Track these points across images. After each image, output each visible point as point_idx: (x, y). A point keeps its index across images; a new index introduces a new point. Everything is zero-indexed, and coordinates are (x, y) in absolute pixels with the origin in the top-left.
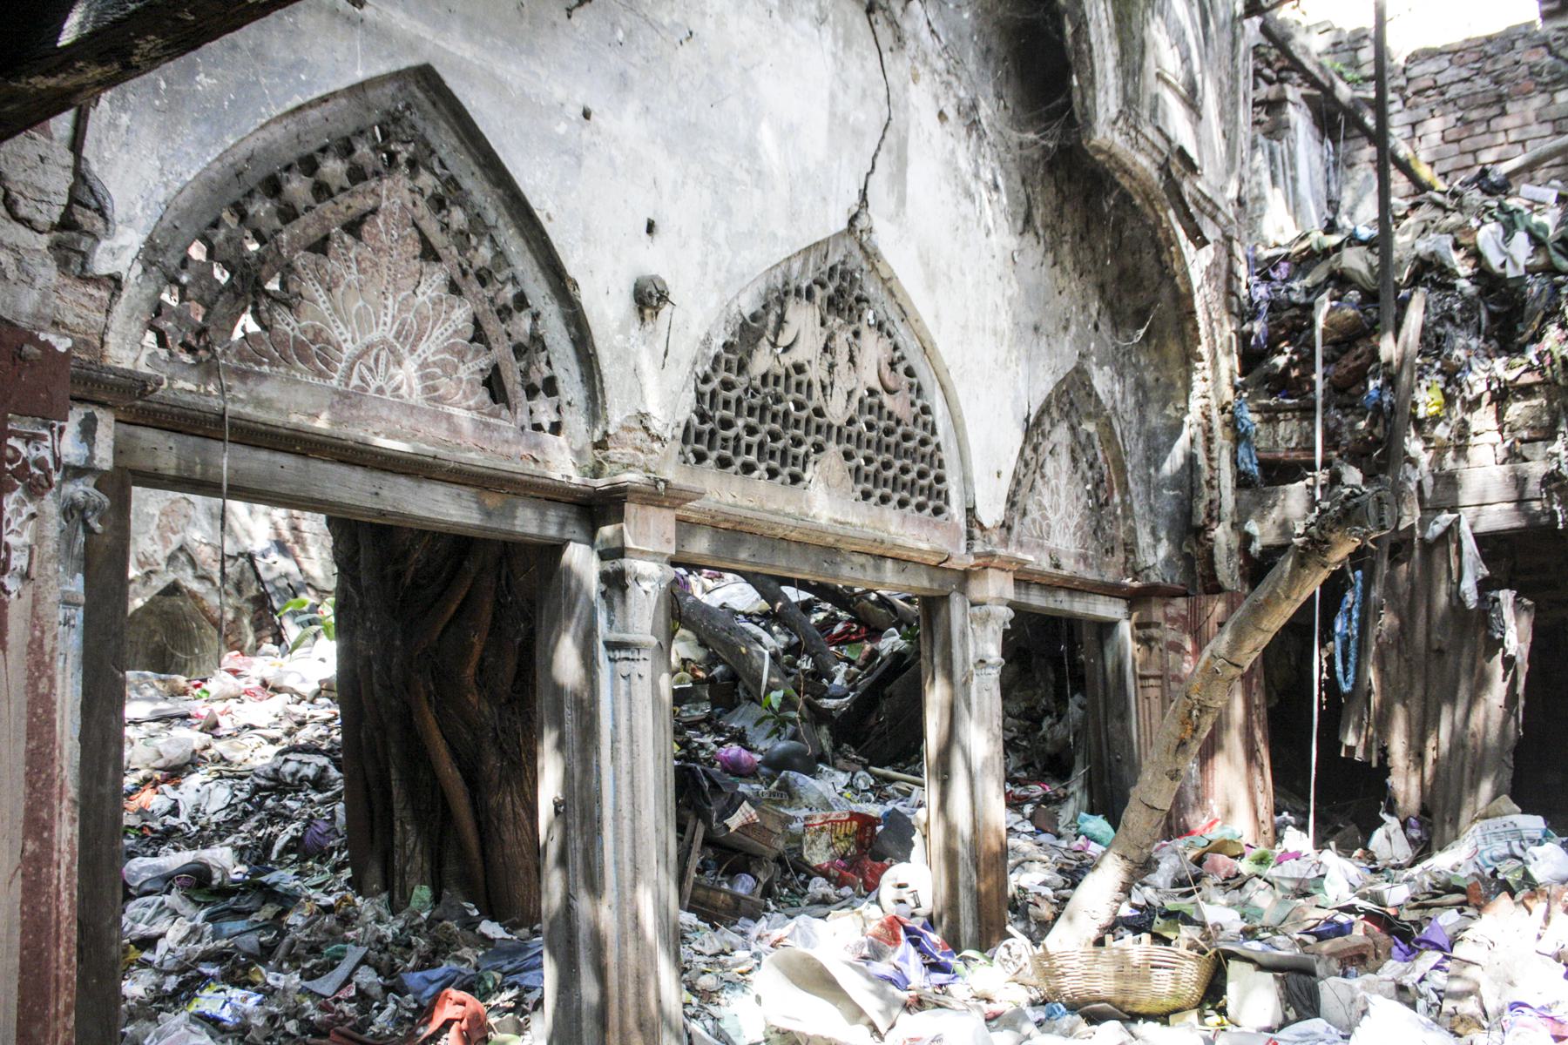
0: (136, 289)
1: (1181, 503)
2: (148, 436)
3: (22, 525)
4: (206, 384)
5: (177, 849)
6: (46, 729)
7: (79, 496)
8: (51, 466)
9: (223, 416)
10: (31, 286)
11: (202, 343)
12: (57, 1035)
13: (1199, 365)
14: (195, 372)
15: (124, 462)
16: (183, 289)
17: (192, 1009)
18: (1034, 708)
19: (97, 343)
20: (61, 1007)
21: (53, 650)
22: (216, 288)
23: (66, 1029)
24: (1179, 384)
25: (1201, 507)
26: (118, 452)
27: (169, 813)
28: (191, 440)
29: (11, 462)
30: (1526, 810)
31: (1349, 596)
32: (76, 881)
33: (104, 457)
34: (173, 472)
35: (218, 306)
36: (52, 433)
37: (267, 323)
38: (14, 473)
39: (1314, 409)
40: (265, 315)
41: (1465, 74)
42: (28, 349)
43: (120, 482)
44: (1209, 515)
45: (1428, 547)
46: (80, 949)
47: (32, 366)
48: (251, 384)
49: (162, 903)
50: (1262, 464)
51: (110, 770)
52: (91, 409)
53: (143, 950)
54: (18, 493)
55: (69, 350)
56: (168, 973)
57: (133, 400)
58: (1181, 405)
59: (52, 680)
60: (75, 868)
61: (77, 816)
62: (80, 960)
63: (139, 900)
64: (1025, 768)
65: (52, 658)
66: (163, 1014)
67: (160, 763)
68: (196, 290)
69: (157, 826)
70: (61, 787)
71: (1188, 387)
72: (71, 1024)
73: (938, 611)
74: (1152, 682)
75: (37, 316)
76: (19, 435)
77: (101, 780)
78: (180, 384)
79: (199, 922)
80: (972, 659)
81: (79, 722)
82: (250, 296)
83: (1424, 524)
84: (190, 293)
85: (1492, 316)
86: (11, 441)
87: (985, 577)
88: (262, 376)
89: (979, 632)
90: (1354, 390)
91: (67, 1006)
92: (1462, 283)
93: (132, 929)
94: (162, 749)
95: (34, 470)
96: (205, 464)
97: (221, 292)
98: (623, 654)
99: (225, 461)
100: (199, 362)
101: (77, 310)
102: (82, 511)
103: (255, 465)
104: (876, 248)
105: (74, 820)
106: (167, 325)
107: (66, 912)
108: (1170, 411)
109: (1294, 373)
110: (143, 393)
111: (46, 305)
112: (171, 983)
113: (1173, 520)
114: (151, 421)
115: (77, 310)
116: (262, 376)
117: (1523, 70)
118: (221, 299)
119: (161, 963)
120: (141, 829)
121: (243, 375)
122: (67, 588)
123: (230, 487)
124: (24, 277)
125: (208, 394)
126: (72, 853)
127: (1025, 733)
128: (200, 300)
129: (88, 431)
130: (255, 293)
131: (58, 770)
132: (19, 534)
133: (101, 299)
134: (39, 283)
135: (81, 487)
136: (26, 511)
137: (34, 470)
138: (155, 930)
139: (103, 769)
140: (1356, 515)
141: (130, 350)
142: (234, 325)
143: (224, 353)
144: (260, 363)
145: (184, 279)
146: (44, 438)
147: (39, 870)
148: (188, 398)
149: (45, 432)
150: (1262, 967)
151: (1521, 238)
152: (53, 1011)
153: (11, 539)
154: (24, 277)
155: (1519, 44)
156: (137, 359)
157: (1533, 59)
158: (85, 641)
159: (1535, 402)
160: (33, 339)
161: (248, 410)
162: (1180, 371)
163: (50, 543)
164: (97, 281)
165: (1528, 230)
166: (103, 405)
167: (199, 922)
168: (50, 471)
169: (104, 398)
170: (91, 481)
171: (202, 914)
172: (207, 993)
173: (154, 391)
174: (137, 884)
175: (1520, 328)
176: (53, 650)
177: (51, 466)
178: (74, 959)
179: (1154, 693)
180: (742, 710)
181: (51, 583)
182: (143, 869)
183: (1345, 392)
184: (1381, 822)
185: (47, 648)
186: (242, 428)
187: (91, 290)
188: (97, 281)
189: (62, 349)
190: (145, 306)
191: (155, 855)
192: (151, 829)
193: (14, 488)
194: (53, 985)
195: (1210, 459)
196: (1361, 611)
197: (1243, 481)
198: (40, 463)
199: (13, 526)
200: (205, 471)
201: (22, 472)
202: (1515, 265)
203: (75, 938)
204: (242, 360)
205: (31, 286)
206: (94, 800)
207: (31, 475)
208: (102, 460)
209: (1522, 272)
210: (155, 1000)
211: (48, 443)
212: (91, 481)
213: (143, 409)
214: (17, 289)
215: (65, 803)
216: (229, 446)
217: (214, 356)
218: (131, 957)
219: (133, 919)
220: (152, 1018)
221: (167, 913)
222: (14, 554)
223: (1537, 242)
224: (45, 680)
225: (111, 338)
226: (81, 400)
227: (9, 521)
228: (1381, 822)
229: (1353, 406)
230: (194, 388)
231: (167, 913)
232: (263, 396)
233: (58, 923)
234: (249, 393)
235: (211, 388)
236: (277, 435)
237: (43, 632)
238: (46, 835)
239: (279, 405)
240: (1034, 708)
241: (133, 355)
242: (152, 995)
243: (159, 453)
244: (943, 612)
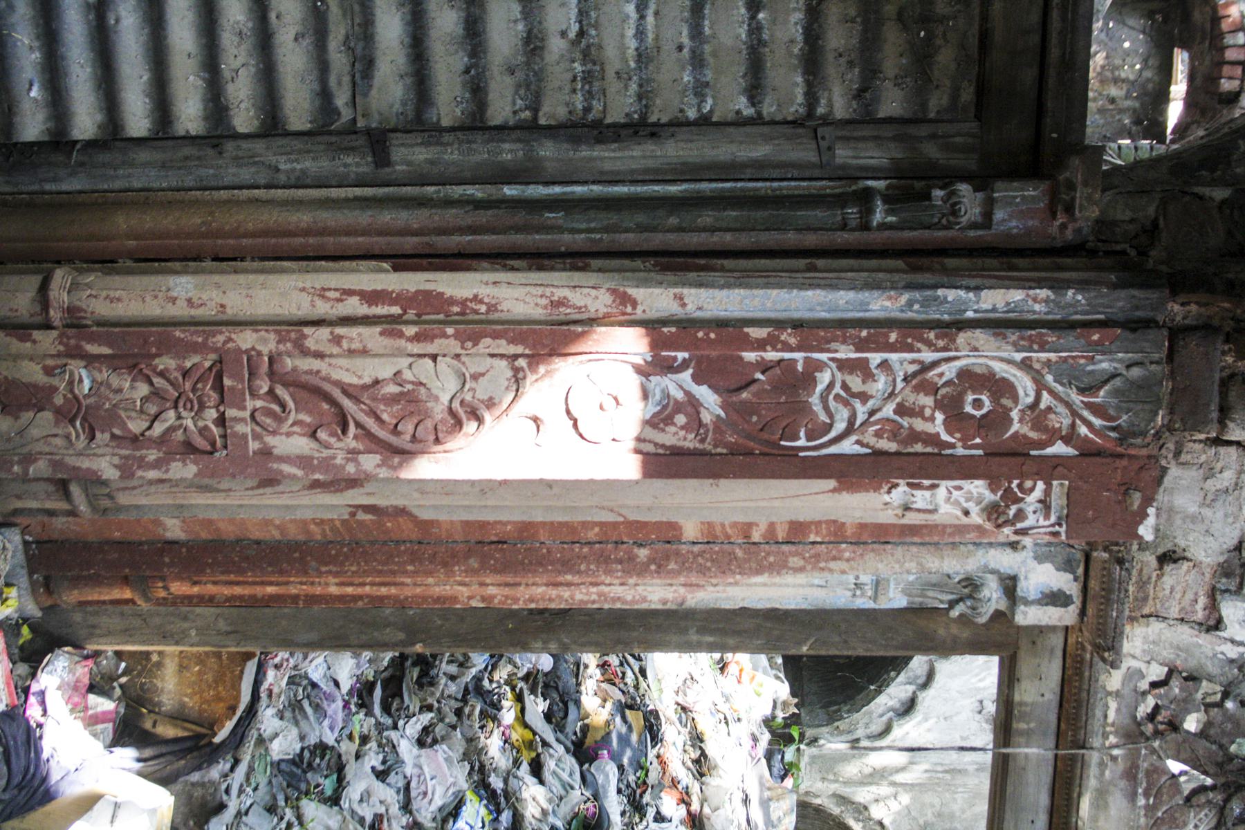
0: (1212, 651)
2: (1053, 671)
3: (957, 503)
4: (1116, 733)
5: (623, 814)
6: (754, 565)
7: (985, 593)
8: (1019, 526)
9: (1083, 747)
10: (1203, 505)
11: (1161, 727)
12: (465, 584)
14: (1127, 721)
15: (1024, 644)
16: (1220, 705)
17: (470, 795)
19: (1146, 611)
20: (492, 590)
21: (831, 570)
22: (1225, 741)
23: (470, 598)
26: (1040, 631)
27: (658, 813)
28: (1053, 718)
29: (1020, 486)
32: (606, 606)
33: (1028, 616)
34: (1017, 698)
35: (1204, 743)
36: (1053, 525)
37: (1194, 801)
38: (1008, 490)
40: (1203, 799)
42: (1136, 499)
43: (1002, 639)
46: (541, 612)
47: (1120, 502)
48: (1123, 784)
49: (572, 788)
51: (711, 639)
52: (1077, 601)
53: (530, 765)
54: (989, 497)
55: (1141, 538)
56: (506, 781)
57: (1091, 642)
59: (801, 570)
60: (618, 606)
61: (668, 606)
62: (531, 611)
63: (577, 767)
65: (822, 569)
66: (468, 767)
67: (706, 810)
68: (1220, 718)
69: (647, 798)
70: (697, 585)
72: (474, 603)
75: (1171, 511)
76: (1047, 492)
77: (702, 630)
78: (1113, 705)
79: (551, 819)
81: (760, 606)
82: (1223, 780)
84: (1215, 711)
86: (1040, 485)
88: (1133, 797)
91: (492, 597)
93: (551, 756)
94: (720, 812)
95: (1013, 510)
96: (1028, 733)
97: (1221, 746)
99: (1034, 750)
100: (1139, 724)
101: (1179, 588)
102: (970, 597)
103: (1031, 790)
105: (665, 603)
106: (1176, 688)
107: (578, 597)
110: (1099, 649)
111: (1184, 520)
112: (496, 783)
114: (1069, 672)
115: (1179, 588)
116: (1133, 797)
118: (1214, 747)
119: (516, 777)
120: (645, 783)
121: (1131, 774)
122: (892, 586)
123: (1006, 758)
124: (1210, 497)
125: (1105, 736)
126: (633, 602)
128: (1208, 724)
129: (1055, 598)
130: (1226, 786)
131: (714, 581)
132: (948, 500)
133: (1195, 612)
134: (1207, 512)
135: (995, 596)
136: (971, 506)
137: (1013, 510)
138: (547, 775)
139: (711, 632)
141: (1145, 649)
142: (1184, 762)
143: (1154, 751)
144: (1147, 794)
145: (1229, 705)
146: (1047, 517)
147: (621, 562)
148: (1098, 713)
149: (1053, 519)
152: (488, 581)
153: (941, 492)
154: (1210, 497)
156: (1134, 657)
158: (840, 612)
160: (1148, 501)
161: (1092, 782)
163: (937, 564)
164: (1213, 606)
166: (1083, 613)
167: (551, 819)
168: (1013, 524)
169: (1090, 611)
170: (1003, 605)
171: (559, 824)
172: (483, 811)
173: (1104, 660)
174: (592, 770)
176: (831, 570)
177: (1019, 526)
178: (533, 606)
180: (953, 375)
181: (897, 566)
182: (607, 776)
185: (832, 565)
186: (1072, 771)
187: (1202, 601)
188: (1213, 606)
189: (1142, 530)
190: (1192, 663)
191: (619, 791)
192: (644, 792)
193: (993, 491)
194: (509, 579)
198: (1020, 515)
199: (956, 493)
200: (1021, 733)
201: (1010, 498)
203: (552, 606)
204: (1148, 774)
205: (1203, 505)
206: (683, 624)
207: (1007, 506)
208: (1025, 614)
210: (482, 766)
211: (1042, 522)
212: (1003, 605)
213: (1082, 662)
214: (1197, 490)
215: (682, 590)
216: (1050, 755)
217: (1148, 739)
218: (525, 752)
219: (559, 760)
220: (466, 756)
221: (563, 793)
222: (927, 494)
224: (801, 563)
225: (1156, 627)
226: (1085, 590)
227: (959, 488)
230: (1110, 720)
231: (563, 793)
232: (1110, 799)
233: (569, 584)
234: (1111, 782)
235: (1113, 739)
236: (1068, 812)
237: (848, 560)
238: (653, 567)
239: (1102, 818)
241: (1138, 652)
242: (487, 763)
243: (1037, 682)
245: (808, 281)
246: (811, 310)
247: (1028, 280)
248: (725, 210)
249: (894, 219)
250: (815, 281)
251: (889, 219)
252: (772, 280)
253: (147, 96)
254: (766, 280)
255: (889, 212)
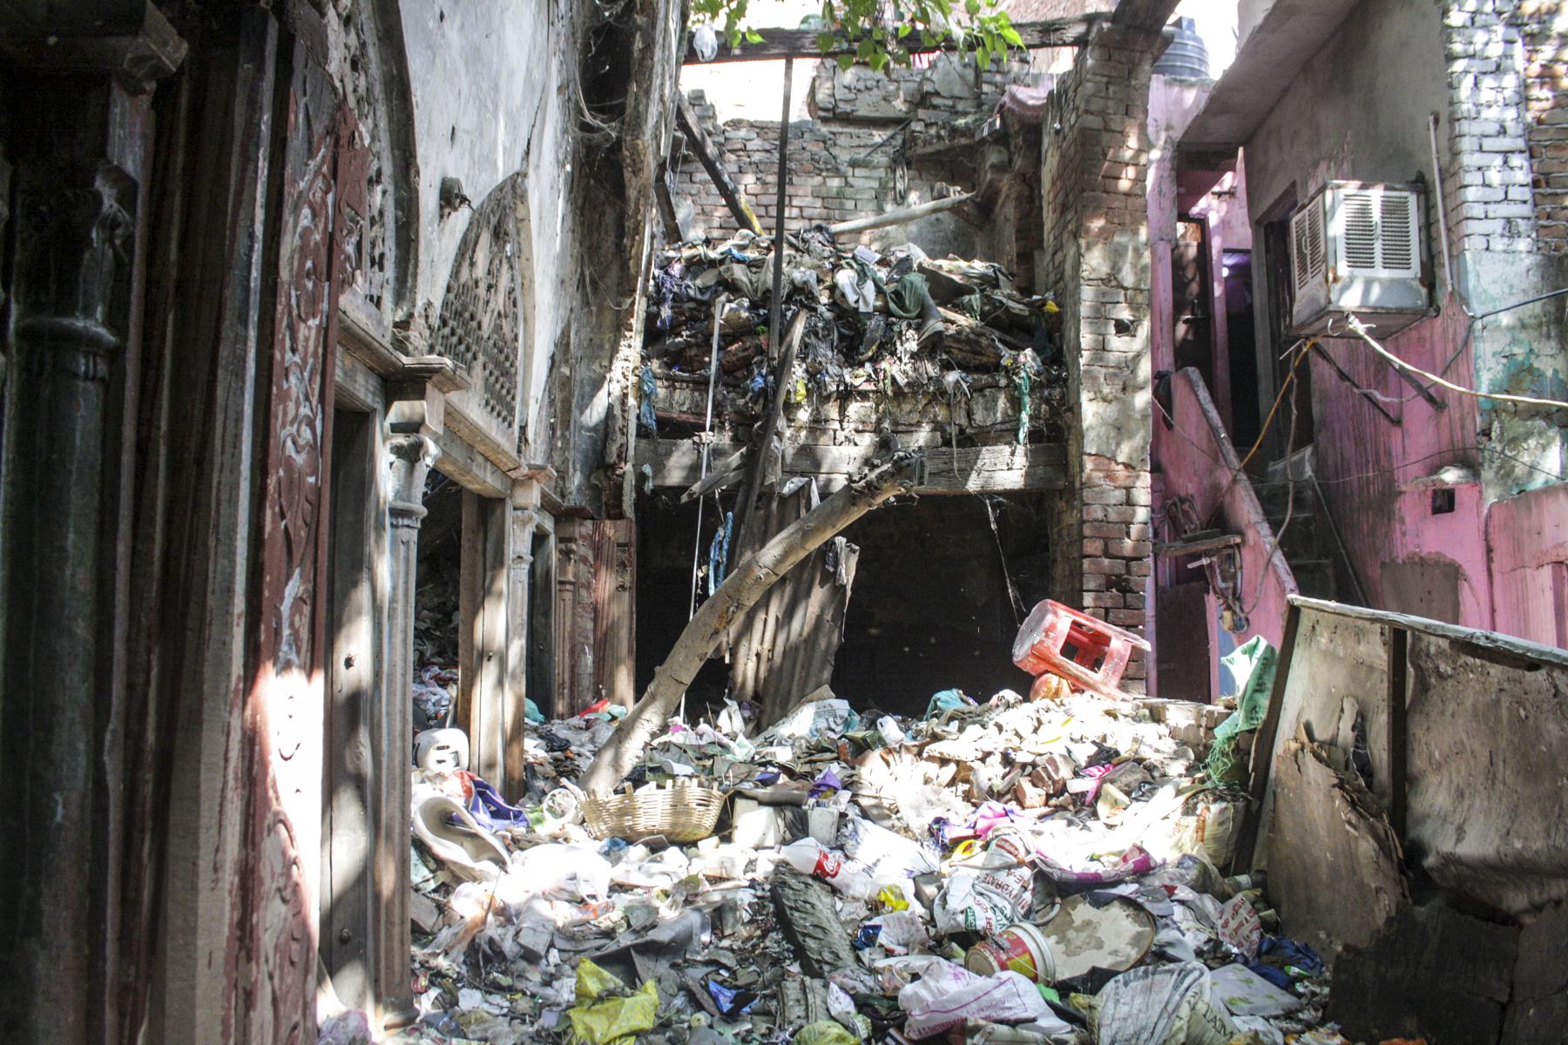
1: (595, 442)
13: (628, 334)
18: (444, 604)
24: (607, 346)
25: (614, 449)
30: (837, 697)
31: (721, 532)
39: (707, 384)
41: (768, 147)
44: (619, 456)
45: (783, 500)
50: (659, 421)
58: (605, 363)
64: (440, 654)
71: (615, 350)
73: (493, 512)
74: (568, 587)
80: (512, 556)
83: (783, 483)
85: (842, 337)
87: (531, 486)
89: (518, 531)
90: (739, 374)
92: (821, 309)
98: (406, 522)
104: (526, 191)
108: (596, 367)
109: (693, 352)
113: (586, 457)
117: (807, 155)
127: (437, 624)
140: (908, 471)
150: (761, 803)
151: (870, 285)
155: (806, 136)
157: (815, 149)
159: (867, 404)
162: (609, 336)
165: (874, 281)
175: (862, 349)
179: (568, 596)
183: (733, 374)
184: (725, 705)
195: (624, 411)
196: (730, 544)
197: (643, 432)
202: (866, 303)
209: (871, 310)
223: (879, 291)
228: (725, 705)
229: (736, 386)
240: (444, 604)
244: (498, 512)
245: (228, 450)
246: (427, 248)
247: (244, 170)
248: (63, 550)
249: (99, 309)
250: (229, 438)
251: (99, 315)
252: (224, 496)
253: (1516, 858)
254: (224, 505)
255: (88, 312)
